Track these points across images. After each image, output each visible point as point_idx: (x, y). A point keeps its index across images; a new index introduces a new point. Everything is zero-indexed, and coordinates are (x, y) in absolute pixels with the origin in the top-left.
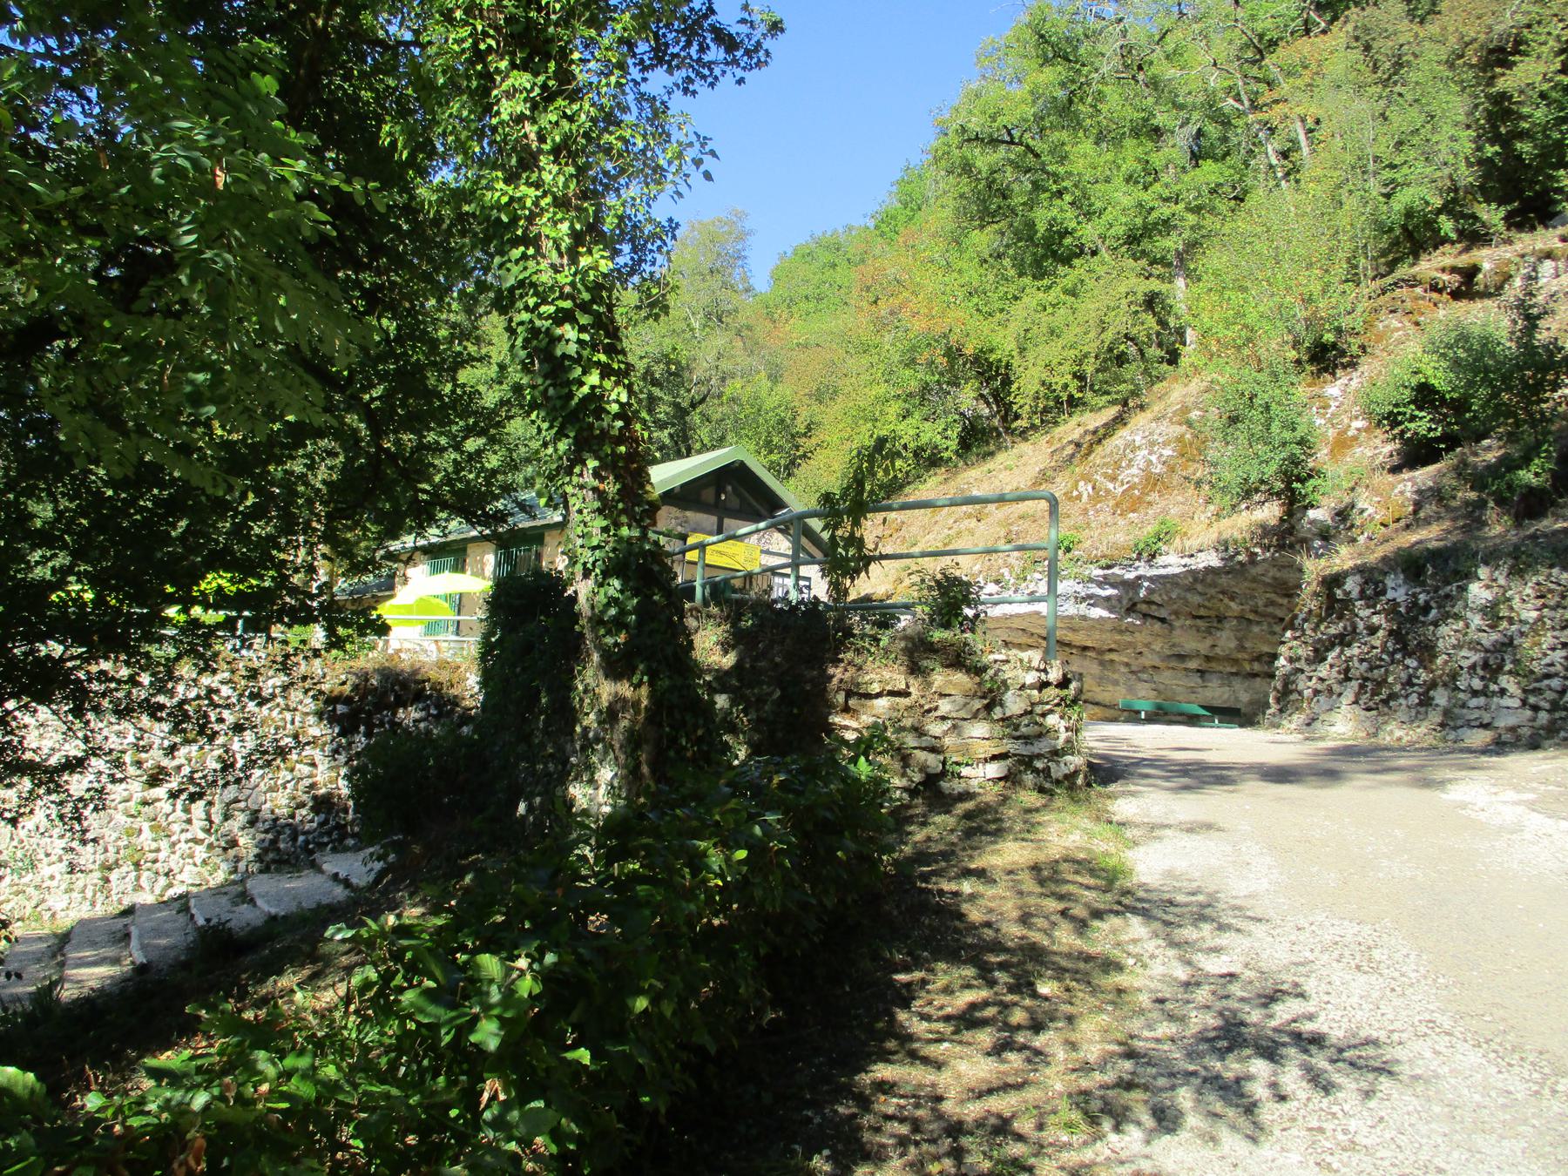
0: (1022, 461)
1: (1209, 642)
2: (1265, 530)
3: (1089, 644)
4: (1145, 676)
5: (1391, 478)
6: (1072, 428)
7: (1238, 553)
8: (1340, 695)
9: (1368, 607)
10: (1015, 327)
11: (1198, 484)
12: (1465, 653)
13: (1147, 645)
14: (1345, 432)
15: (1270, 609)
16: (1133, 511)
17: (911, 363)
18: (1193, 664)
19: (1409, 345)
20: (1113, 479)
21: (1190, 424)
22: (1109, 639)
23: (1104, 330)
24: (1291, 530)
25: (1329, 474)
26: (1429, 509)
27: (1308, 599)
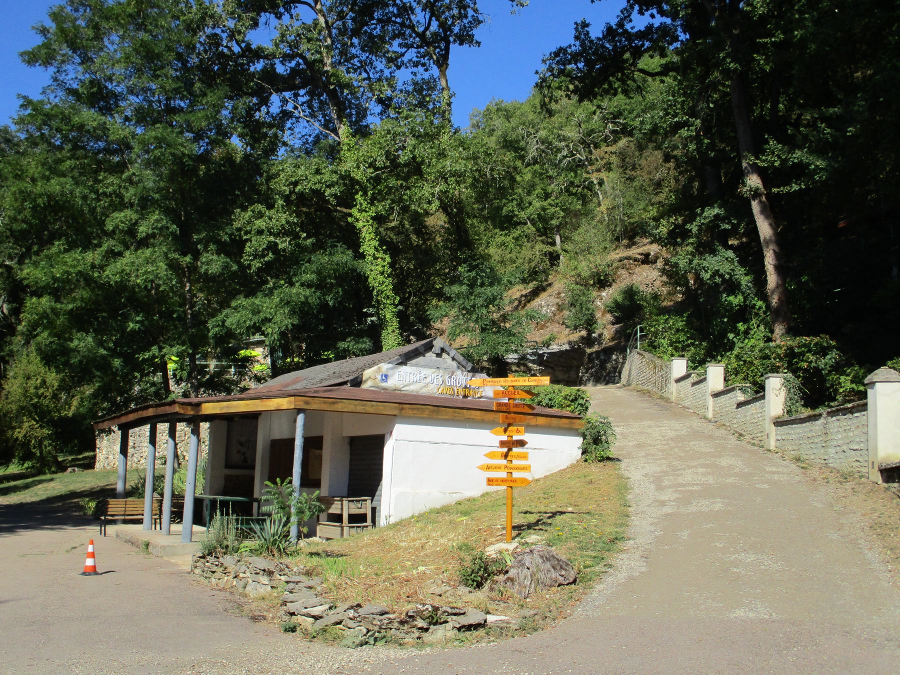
2: (582, 337)
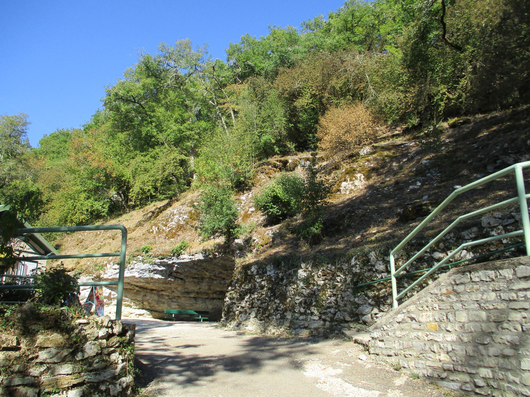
0: (132, 217)
1: (198, 287)
2: (219, 246)
3: (154, 288)
4: (175, 300)
5: (264, 229)
6: (152, 207)
7: (210, 255)
8: (250, 314)
9: (260, 278)
10: (131, 168)
11: (196, 229)
12: (297, 298)
13: (176, 288)
14: (247, 212)
15: (220, 275)
16: (173, 238)
17: (91, 178)
18: (192, 295)
19: (268, 183)
20: (166, 226)
21: (194, 206)
22: (162, 286)
23: (164, 171)
24: (229, 247)
25: (242, 227)
26: (278, 241)
27: (237, 274)
